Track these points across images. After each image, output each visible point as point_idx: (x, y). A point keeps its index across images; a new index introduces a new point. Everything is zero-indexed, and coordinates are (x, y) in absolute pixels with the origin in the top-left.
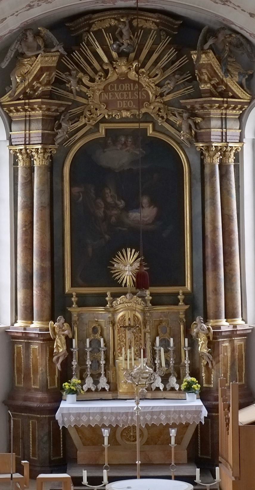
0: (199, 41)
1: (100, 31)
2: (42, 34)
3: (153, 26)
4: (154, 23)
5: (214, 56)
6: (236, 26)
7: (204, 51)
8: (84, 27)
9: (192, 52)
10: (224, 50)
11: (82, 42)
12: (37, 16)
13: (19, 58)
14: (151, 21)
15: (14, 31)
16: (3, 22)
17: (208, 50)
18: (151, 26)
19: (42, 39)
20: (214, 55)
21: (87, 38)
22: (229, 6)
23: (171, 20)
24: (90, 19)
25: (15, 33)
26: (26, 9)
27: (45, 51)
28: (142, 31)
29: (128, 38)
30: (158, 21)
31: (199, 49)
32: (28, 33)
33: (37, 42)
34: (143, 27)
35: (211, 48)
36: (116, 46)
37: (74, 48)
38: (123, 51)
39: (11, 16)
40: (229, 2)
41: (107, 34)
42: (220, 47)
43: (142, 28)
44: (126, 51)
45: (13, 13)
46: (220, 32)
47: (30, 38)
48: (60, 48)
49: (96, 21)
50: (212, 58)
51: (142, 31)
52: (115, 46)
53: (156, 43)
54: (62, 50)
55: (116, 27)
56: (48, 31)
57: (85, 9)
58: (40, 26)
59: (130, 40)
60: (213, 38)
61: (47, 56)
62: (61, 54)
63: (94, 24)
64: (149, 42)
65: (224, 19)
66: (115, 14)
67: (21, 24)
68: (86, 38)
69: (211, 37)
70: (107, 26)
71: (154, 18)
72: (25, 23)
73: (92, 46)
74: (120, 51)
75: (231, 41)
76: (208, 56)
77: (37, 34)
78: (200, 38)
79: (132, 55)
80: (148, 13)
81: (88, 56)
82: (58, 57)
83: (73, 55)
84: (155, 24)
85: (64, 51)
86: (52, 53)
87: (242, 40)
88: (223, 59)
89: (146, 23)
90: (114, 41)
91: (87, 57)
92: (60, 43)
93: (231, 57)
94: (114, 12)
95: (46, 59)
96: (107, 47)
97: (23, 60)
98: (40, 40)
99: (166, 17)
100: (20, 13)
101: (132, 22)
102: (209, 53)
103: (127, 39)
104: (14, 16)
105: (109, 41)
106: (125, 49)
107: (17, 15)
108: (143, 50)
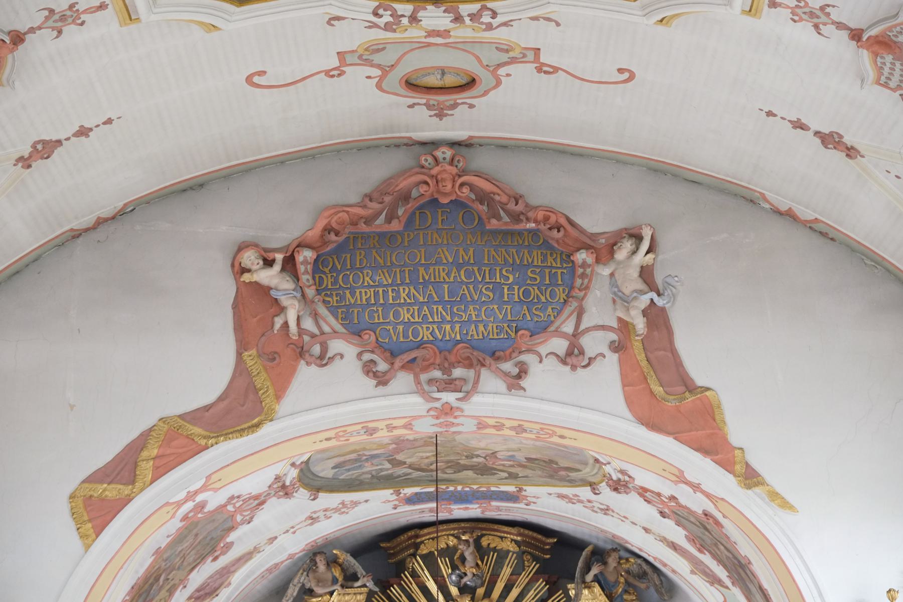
0: (578, 569)
1: (431, 553)
2: (340, 560)
3: (512, 547)
4: (513, 542)
5: (602, 592)
6: (632, 546)
7: (587, 584)
8: (407, 548)
9: (569, 586)
10: (617, 582)
11: (404, 572)
12: (331, 533)
13: (306, 597)
14: (509, 539)
15: (297, 556)
16: (272, 543)
17: (593, 583)
18: (508, 546)
19: (339, 568)
20: (600, 590)
21: (412, 566)
22: (612, 516)
23: (539, 537)
24: (417, 536)
25: (300, 559)
26: (307, 524)
27: (342, 586)
28: (496, 554)
29: (473, 564)
30: (519, 538)
31: (579, 581)
32: (318, 559)
33: (332, 573)
34: (497, 548)
35: (596, 579)
36: (456, 577)
37: (392, 581)
38: (465, 584)
39: (284, 533)
40: (610, 511)
41: (443, 559)
42: (611, 578)
43: (495, 550)
44: (471, 584)
45: (286, 529)
46: (610, 556)
47: (322, 567)
48: (368, 581)
49: (426, 540)
50: (598, 595)
51: (496, 554)
52: (454, 578)
53: (516, 573)
54: (371, 584)
55: (455, 549)
56: (349, 555)
57: (408, 521)
58: (335, 548)
59: (477, 568)
60: (599, 564)
61: (349, 594)
62: (370, 590)
63: (423, 544)
64: (506, 572)
65: (614, 536)
66: (454, 529)
67: (307, 545)
68: (411, 565)
69: (595, 563)
70: (442, 546)
71: (513, 534)
72: (313, 544)
73: (420, 577)
74: (462, 585)
75: (628, 568)
76: (593, 593)
77: (332, 562)
78: (580, 564)
79: (481, 591)
80: (504, 527)
81: (413, 592)
82: (366, 594)
83: (391, 591)
84: (516, 544)
85: (375, 586)
86: (356, 589)
87: (645, 567)
88: (616, 596)
89: (501, 542)
90: (452, 570)
91: (413, 595)
92: (367, 573)
93: (630, 593)
94: (452, 526)
95: (346, 598)
96: (443, 578)
97: (311, 599)
98: (337, 569)
99: (530, 533)
100: (299, 529)
101: (480, 540)
102: (594, 587)
103: (472, 567)
104: (289, 535)
105: (445, 570)
106: (469, 581)
107: (294, 533)
108: (496, 583)
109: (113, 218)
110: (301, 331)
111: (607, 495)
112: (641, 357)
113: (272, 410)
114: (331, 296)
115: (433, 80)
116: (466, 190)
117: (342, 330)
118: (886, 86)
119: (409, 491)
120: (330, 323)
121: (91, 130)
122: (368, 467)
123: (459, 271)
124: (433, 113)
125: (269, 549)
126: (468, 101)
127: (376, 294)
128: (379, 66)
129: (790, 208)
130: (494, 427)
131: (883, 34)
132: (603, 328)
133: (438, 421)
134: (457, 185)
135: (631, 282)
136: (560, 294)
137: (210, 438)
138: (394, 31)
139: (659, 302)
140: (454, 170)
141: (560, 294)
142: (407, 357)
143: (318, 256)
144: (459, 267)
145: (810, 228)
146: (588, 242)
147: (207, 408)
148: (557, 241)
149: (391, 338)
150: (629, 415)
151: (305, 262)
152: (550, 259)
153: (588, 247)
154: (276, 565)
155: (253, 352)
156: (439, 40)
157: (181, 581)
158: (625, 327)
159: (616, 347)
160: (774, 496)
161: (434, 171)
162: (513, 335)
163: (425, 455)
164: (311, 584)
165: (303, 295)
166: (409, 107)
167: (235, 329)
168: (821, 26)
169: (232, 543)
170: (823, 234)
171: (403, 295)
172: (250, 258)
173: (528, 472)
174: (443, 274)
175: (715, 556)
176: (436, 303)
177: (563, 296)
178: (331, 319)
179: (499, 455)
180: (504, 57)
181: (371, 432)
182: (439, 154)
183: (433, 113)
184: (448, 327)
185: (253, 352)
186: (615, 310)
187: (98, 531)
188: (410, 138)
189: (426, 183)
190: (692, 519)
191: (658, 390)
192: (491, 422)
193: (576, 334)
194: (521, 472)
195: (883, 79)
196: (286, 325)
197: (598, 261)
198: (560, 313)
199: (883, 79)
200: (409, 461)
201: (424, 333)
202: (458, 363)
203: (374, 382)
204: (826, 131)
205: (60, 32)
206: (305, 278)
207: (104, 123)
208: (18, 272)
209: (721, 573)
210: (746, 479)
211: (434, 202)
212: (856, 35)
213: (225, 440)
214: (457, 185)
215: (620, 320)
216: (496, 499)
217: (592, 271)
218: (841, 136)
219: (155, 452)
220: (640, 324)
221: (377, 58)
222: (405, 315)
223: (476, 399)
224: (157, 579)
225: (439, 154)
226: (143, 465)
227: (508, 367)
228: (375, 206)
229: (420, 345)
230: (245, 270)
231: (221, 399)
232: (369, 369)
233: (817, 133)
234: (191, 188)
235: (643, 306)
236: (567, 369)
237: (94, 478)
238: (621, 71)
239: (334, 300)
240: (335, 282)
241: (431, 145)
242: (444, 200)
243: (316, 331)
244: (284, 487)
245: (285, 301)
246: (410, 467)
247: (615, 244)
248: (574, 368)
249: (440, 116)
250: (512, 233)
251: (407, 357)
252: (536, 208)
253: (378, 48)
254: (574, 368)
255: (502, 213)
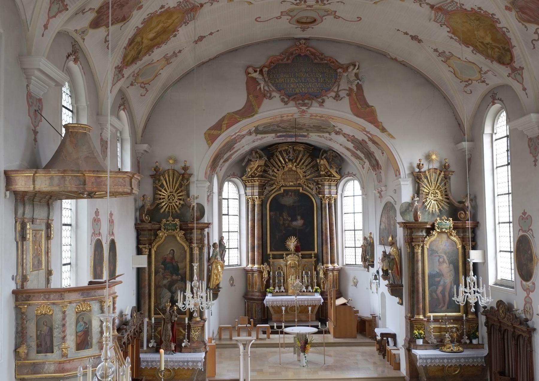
8: (275, 149)
9: (317, 159)
10: (330, 158)
24: (277, 146)
25: (248, 152)
27: (259, 159)
35: (325, 158)
42: (329, 157)
43: (298, 150)
47: (254, 154)
53: (303, 156)
54: (266, 159)
55: (287, 149)
58: (258, 149)
64: (301, 156)
77: (256, 152)
79: (294, 161)
87: (337, 154)
94: (287, 144)
104: (247, 145)
105: (285, 155)
109: (213, 59)
110: (264, 90)
111: (333, 135)
112: (355, 98)
113: (257, 111)
114: (272, 80)
115: (304, 20)
116: (308, 52)
117: (275, 90)
118: (436, 22)
119: (279, 134)
120: (272, 88)
121: (213, 33)
122: (272, 128)
123: (307, 74)
124: (301, 30)
125: (242, 149)
126: (312, 26)
127: (284, 80)
128: (291, 16)
129: (396, 58)
130: (315, 116)
131: (441, 6)
132: (345, 90)
133: (300, 114)
134: (306, 50)
135: (353, 77)
136: (333, 80)
137: (240, 118)
138: (298, 5)
139: (360, 83)
140: (305, 46)
141: (333, 80)
142: (293, 97)
143: (269, 70)
144: (307, 73)
145: (401, 63)
146: (341, 66)
147: (240, 110)
148: (333, 66)
149: (288, 92)
150: (351, 113)
151: (265, 71)
152: (331, 71)
153: (341, 68)
154: (242, 153)
155: (252, 95)
156: (310, 8)
157: (223, 157)
158: (351, 90)
159: (348, 95)
160: (389, 135)
161: (300, 47)
162: (321, 91)
163: (286, 124)
164: (251, 158)
165: (265, 80)
166: (296, 28)
167: (247, 89)
168: (422, 4)
169: (235, 147)
170: (404, 65)
171: (292, 80)
172: (250, 70)
173: (312, 129)
174: (302, 75)
175: (361, 151)
176: (300, 83)
177: (334, 81)
178: (272, 87)
179: (306, 125)
180: (326, 13)
181: (282, 117)
182: (301, 42)
183: (301, 30)
184: (304, 89)
185: (252, 95)
186: (348, 85)
187: (212, 143)
188: (293, 37)
189: (298, 50)
190: (357, 142)
191: (359, 106)
192: (314, 115)
193: (338, 91)
194: (310, 129)
195: (436, 19)
196: (260, 88)
197: (344, 72)
198: (333, 86)
199: (436, 19)
200: (282, 126)
201: (297, 91)
202: (306, 99)
203: (284, 104)
204: (413, 35)
205: (212, 4)
206: (265, 76)
207: (217, 31)
208: (188, 74)
209: (362, 156)
210: (383, 130)
211: (299, 55)
212: (432, 7)
213: (245, 119)
214: (306, 50)
215: (349, 88)
216: (300, 137)
217: (342, 74)
218: (418, 37)
219: (226, 122)
220: (355, 89)
221: (291, 14)
222: (292, 86)
223: (311, 108)
224: (218, 156)
225: (301, 42)
226: (223, 125)
227: (319, 100)
228: (284, 56)
229: (296, 94)
230: (249, 73)
231: (243, 108)
232: (282, 100)
233: (411, 36)
234: (234, 51)
235: (356, 84)
236: (335, 101)
237: (211, 129)
238: (358, 18)
239: (273, 82)
240: (273, 77)
241: (299, 39)
242: (302, 55)
243: (268, 90)
244: (250, 132)
245: (260, 82)
246: (282, 128)
247: (348, 67)
248: (337, 100)
249: (303, 31)
250: (320, 64)
251: (293, 97)
252: (327, 57)
253: (292, 10)
254: (337, 100)
255: (318, 58)
